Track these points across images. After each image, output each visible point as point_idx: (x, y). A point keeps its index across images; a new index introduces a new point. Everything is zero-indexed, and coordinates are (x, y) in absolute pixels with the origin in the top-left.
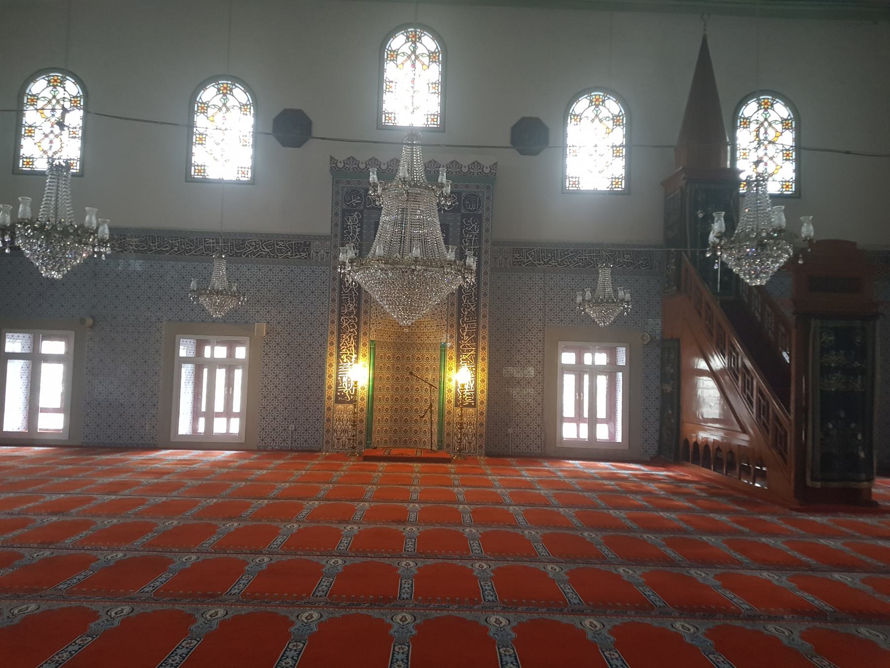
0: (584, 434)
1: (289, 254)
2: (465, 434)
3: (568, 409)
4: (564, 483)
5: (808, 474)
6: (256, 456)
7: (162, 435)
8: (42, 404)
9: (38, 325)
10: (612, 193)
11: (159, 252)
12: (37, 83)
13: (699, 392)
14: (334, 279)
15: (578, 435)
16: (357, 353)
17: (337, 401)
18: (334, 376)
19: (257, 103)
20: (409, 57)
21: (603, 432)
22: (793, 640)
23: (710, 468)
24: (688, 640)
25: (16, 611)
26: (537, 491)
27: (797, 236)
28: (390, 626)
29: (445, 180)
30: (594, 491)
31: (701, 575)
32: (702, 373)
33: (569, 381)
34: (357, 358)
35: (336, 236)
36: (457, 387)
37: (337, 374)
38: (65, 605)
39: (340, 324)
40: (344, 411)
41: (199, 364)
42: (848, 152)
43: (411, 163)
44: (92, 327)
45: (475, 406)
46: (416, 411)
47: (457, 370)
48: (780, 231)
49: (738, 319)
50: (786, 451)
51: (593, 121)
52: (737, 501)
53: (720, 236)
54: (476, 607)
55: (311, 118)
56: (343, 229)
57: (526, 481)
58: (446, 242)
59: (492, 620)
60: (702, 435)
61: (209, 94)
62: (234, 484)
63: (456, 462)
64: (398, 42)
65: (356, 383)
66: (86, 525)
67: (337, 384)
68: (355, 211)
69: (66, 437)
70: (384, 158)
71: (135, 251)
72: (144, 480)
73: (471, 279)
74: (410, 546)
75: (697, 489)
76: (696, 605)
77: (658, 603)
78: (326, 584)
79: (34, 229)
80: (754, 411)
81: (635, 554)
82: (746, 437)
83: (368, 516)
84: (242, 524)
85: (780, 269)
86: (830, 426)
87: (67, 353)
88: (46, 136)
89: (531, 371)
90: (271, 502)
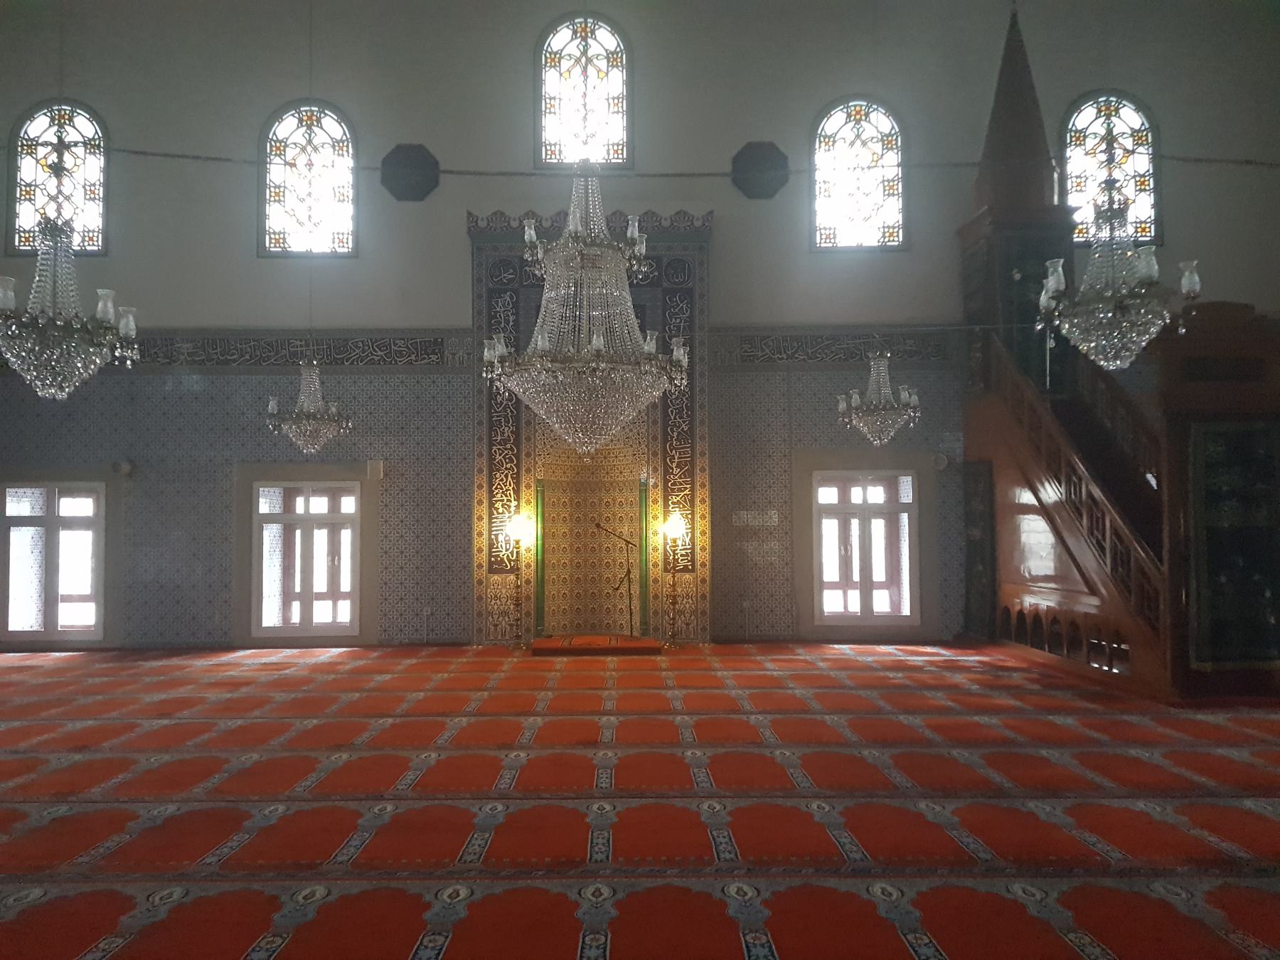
0: (855, 606)
1: (413, 357)
2: (682, 612)
3: (831, 571)
4: (829, 677)
5: (1192, 654)
6: (376, 654)
7: (240, 629)
8: (63, 589)
9: (54, 475)
10: (883, 249)
11: (227, 362)
12: (36, 122)
13: (1024, 538)
14: (480, 392)
15: (846, 607)
16: (518, 499)
17: (491, 570)
18: (485, 533)
19: (358, 139)
20: (578, 61)
21: (881, 603)
22: (1195, 905)
23: (1042, 648)
24: (1032, 910)
26: (790, 692)
27: (1175, 292)
28: (577, 905)
29: (636, 234)
31: (1043, 809)
32: (1027, 509)
33: (830, 528)
34: (518, 507)
35: (480, 328)
36: (665, 544)
37: (490, 532)
38: (86, 888)
39: (491, 458)
40: (502, 584)
41: (289, 523)
42: (1248, 162)
43: (584, 213)
44: (130, 475)
45: (693, 570)
48: (1149, 283)
49: (1076, 424)
50: (1157, 619)
51: (852, 144)
52: (1093, 697)
53: (1058, 296)
54: (708, 870)
55: (439, 158)
56: (491, 317)
57: (772, 677)
58: (643, 330)
59: (732, 890)
60: (1029, 601)
61: (287, 128)
63: (668, 653)
64: (562, 39)
65: (517, 542)
66: (123, 765)
67: (491, 546)
68: (505, 282)
69: (100, 636)
70: (547, 211)
71: (187, 362)
73: (682, 381)
74: (604, 780)
75: (1026, 679)
76: (1040, 856)
77: (982, 855)
78: (479, 842)
79: (21, 326)
80: (1108, 561)
81: (943, 783)
82: (1095, 601)
83: (541, 738)
84: (355, 756)
85: (1150, 343)
86: (1223, 579)
87: (96, 514)
89: (774, 518)
90: (398, 720)
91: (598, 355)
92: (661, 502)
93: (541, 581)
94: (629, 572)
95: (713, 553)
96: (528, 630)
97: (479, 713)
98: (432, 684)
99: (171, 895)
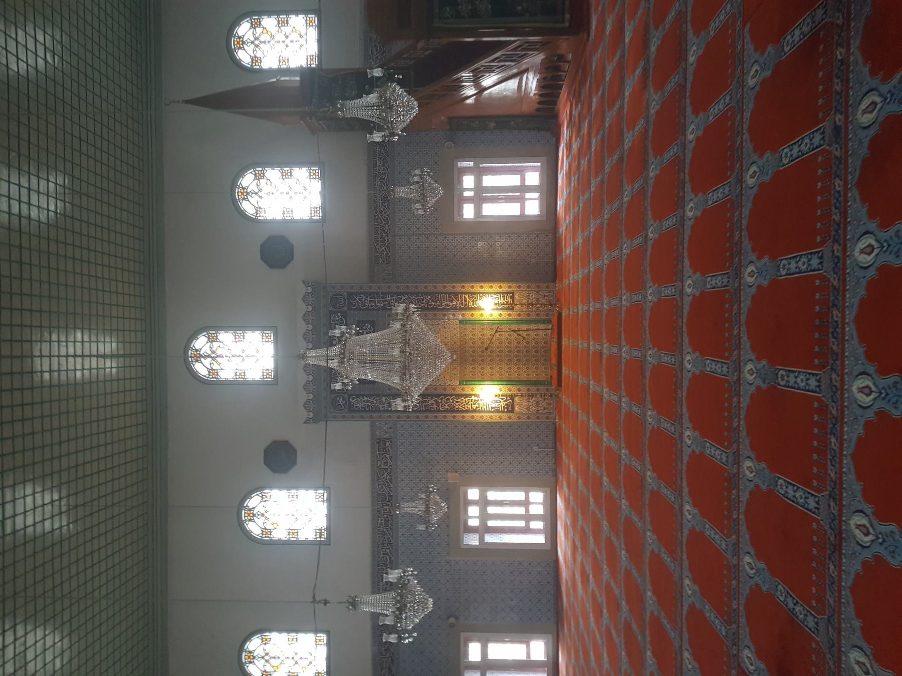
2: (538, 300)
8: (523, 657)
16: (471, 395)
17: (513, 411)
18: (491, 414)
21: (533, 178)
25: (690, 667)
30: (579, 197)
34: (475, 395)
36: (497, 309)
37: (489, 412)
39: (447, 411)
40: (520, 405)
44: (457, 618)
45: (513, 293)
46: (518, 343)
47: (482, 309)
49: (432, 74)
51: (261, 197)
56: (365, 411)
61: (254, 528)
62: (580, 488)
63: (560, 308)
64: (201, 369)
69: (550, 636)
72: (579, 558)
83: (598, 380)
86: (519, 8)
87: (479, 641)
88: (296, 662)
91: (402, 352)
92: (473, 312)
93: (518, 382)
94: (514, 331)
95: (503, 281)
96: (547, 390)
97: (588, 413)
98: (597, 471)
99: (748, 657)
